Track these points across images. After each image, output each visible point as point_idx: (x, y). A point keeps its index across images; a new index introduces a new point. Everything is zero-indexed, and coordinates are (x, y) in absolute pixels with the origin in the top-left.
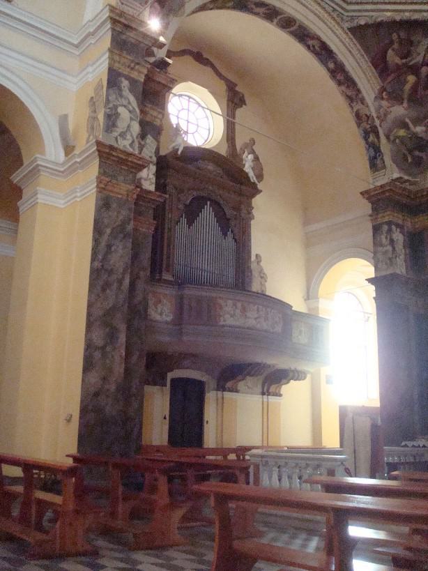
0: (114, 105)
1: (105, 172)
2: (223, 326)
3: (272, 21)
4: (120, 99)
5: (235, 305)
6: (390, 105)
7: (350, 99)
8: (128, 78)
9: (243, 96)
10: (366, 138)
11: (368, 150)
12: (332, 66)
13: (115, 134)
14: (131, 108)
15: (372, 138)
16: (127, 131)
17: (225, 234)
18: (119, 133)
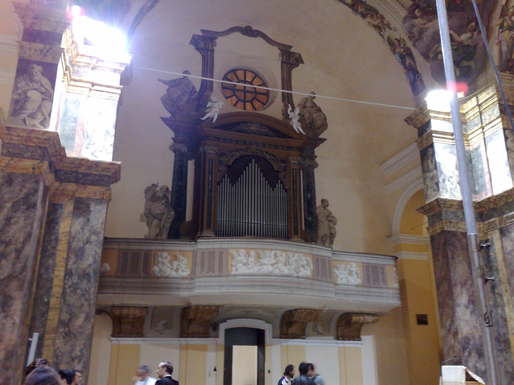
0: (23, 91)
1: (9, 152)
2: (235, 275)
4: (30, 84)
5: (248, 254)
6: (426, 22)
7: (378, 28)
8: (39, 63)
9: (300, 55)
10: (403, 63)
11: (408, 74)
13: (23, 116)
14: (43, 90)
15: (408, 61)
16: (37, 111)
17: (273, 186)
18: (27, 115)
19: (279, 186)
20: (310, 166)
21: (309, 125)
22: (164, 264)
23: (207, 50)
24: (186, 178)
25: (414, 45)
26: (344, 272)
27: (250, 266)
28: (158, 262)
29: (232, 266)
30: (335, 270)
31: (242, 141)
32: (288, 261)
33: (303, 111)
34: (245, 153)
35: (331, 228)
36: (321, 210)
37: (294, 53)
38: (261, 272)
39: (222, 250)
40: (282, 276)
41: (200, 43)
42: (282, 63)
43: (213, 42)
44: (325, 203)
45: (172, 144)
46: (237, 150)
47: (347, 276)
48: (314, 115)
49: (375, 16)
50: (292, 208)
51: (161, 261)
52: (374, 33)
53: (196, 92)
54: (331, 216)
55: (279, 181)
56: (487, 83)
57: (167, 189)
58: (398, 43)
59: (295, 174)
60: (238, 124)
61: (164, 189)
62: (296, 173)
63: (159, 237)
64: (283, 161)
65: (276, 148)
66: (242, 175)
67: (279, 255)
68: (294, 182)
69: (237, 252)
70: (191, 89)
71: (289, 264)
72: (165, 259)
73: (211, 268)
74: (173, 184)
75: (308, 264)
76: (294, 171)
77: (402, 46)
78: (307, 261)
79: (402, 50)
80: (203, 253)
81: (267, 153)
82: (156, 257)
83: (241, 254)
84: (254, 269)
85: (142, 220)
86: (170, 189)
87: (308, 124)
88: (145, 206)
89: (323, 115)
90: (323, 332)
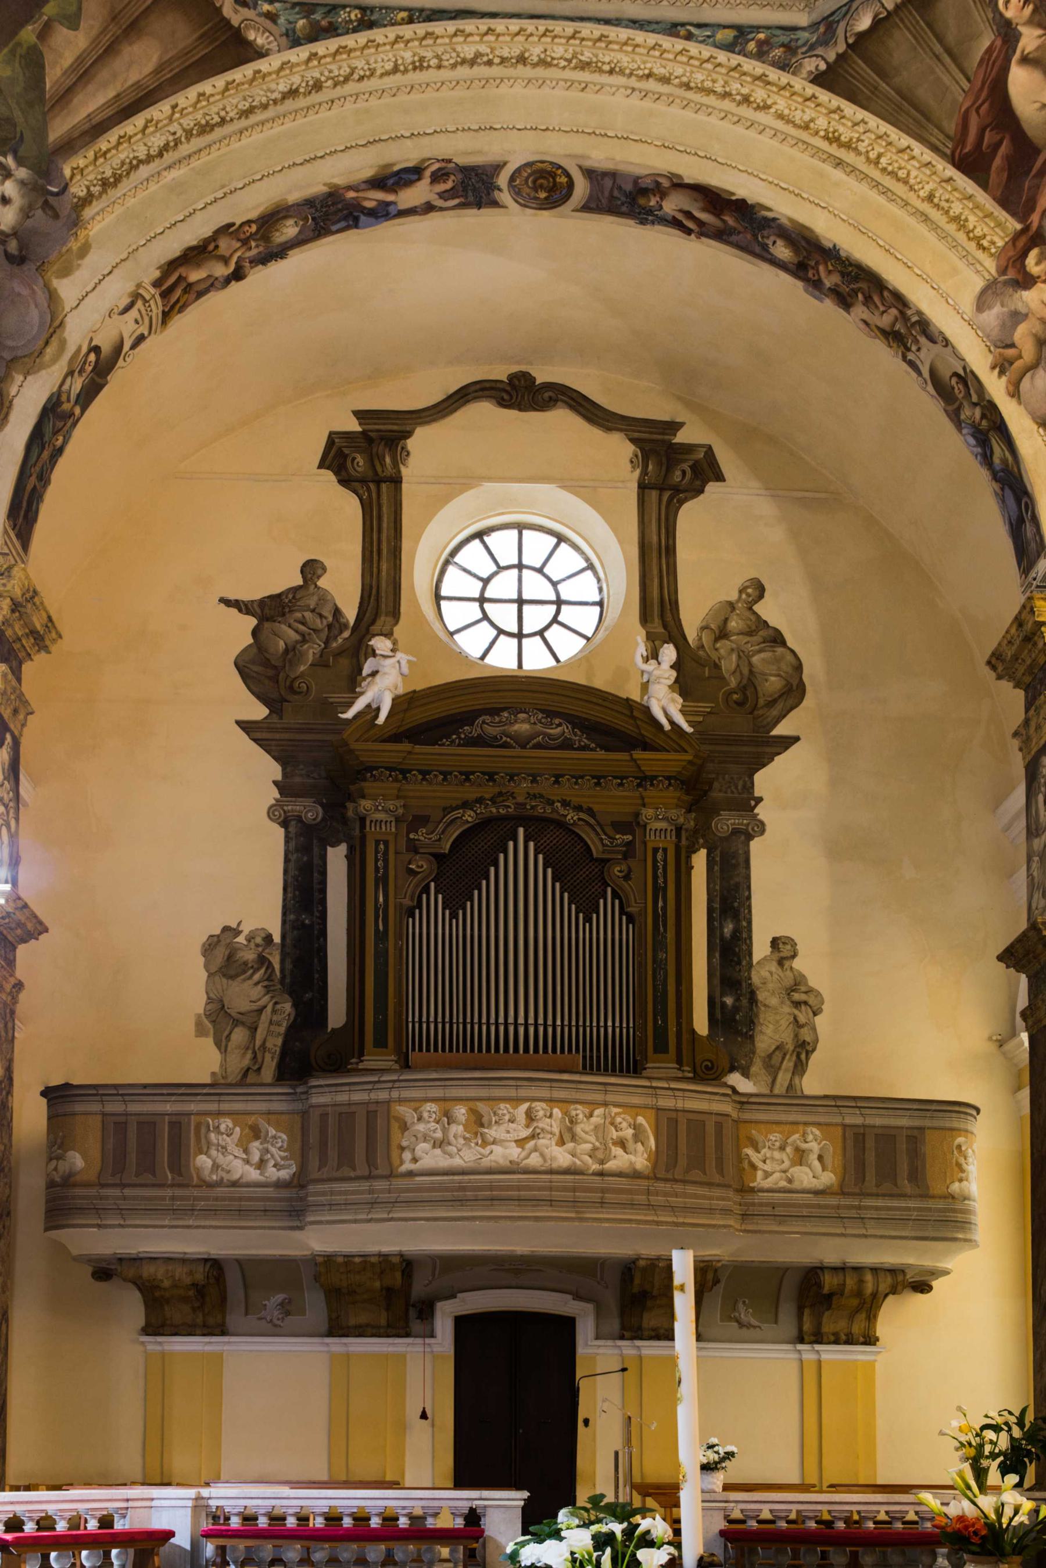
2: (411, 1174)
3: (495, 204)
7: (894, 337)
12: (782, 251)
17: (588, 909)
19: (608, 905)
20: (736, 832)
21: (735, 697)
22: (224, 1148)
23: (378, 482)
24: (323, 902)
25: (1015, 392)
26: (777, 1155)
27: (452, 1149)
28: (209, 1144)
29: (403, 1149)
30: (749, 1151)
31: (484, 773)
32: (570, 1130)
33: (716, 649)
34: (494, 810)
35: (801, 1026)
36: (771, 973)
37: (688, 449)
38: (486, 1163)
39: (372, 1108)
40: (551, 1172)
41: (354, 459)
42: (642, 487)
43: (399, 448)
44: (786, 951)
45: (277, 800)
46: (465, 805)
47: (787, 1163)
48: (755, 660)
49: (876, 299)
50: (650, 972)
51: (215, 1141)
52: (885, 356)
53: (345, 626)
54: (803, 989)
55: (609, 890)
56: (412, 698)
57: (268, 938)
58: (961, 386)
59: (660, 865)
60: (468, 718)
61: (259, 940)
62: (665, 860)
63: (251, 1078)
64: (621, 827)
65: (598, 784)
66: (484, 882)
67: (541, 1113)
68: (659, 890)
69: (415, 1110)
70: (330, 619)
71: (574, 1138)
72: (228, 1136)
73: (346, 1158)
74: (284, 922)
75: (638, 1137)
76: (659, 856)
77: (975, 399)
78: (636, 1127)
79: (978, 412)
80: (324, 1116)
81: (565, 804)
82: (203, 1130)
83: (425, 1115)
84: (466, 1156)
85: (200, 1031)
86: (277, 939)
87: (730, 693)
88: (207, 993)
89: (789, 657)
90: (757, 1323)
